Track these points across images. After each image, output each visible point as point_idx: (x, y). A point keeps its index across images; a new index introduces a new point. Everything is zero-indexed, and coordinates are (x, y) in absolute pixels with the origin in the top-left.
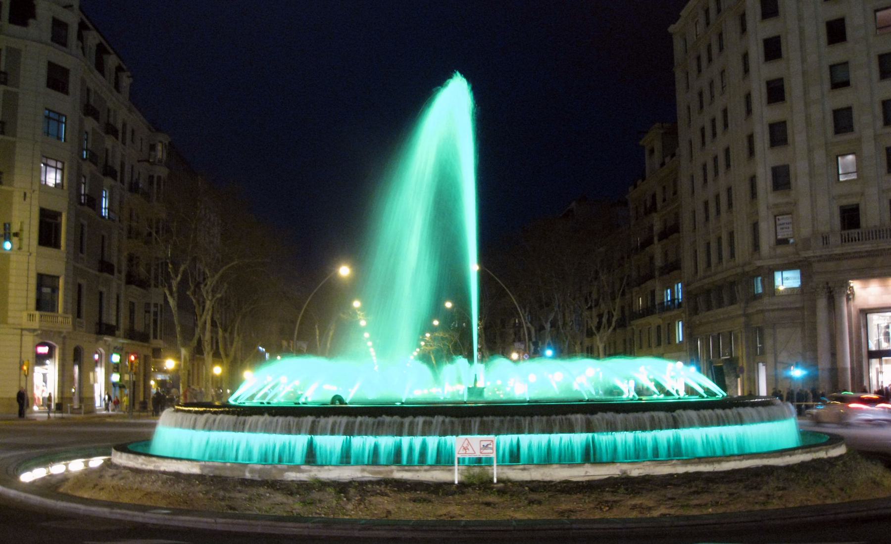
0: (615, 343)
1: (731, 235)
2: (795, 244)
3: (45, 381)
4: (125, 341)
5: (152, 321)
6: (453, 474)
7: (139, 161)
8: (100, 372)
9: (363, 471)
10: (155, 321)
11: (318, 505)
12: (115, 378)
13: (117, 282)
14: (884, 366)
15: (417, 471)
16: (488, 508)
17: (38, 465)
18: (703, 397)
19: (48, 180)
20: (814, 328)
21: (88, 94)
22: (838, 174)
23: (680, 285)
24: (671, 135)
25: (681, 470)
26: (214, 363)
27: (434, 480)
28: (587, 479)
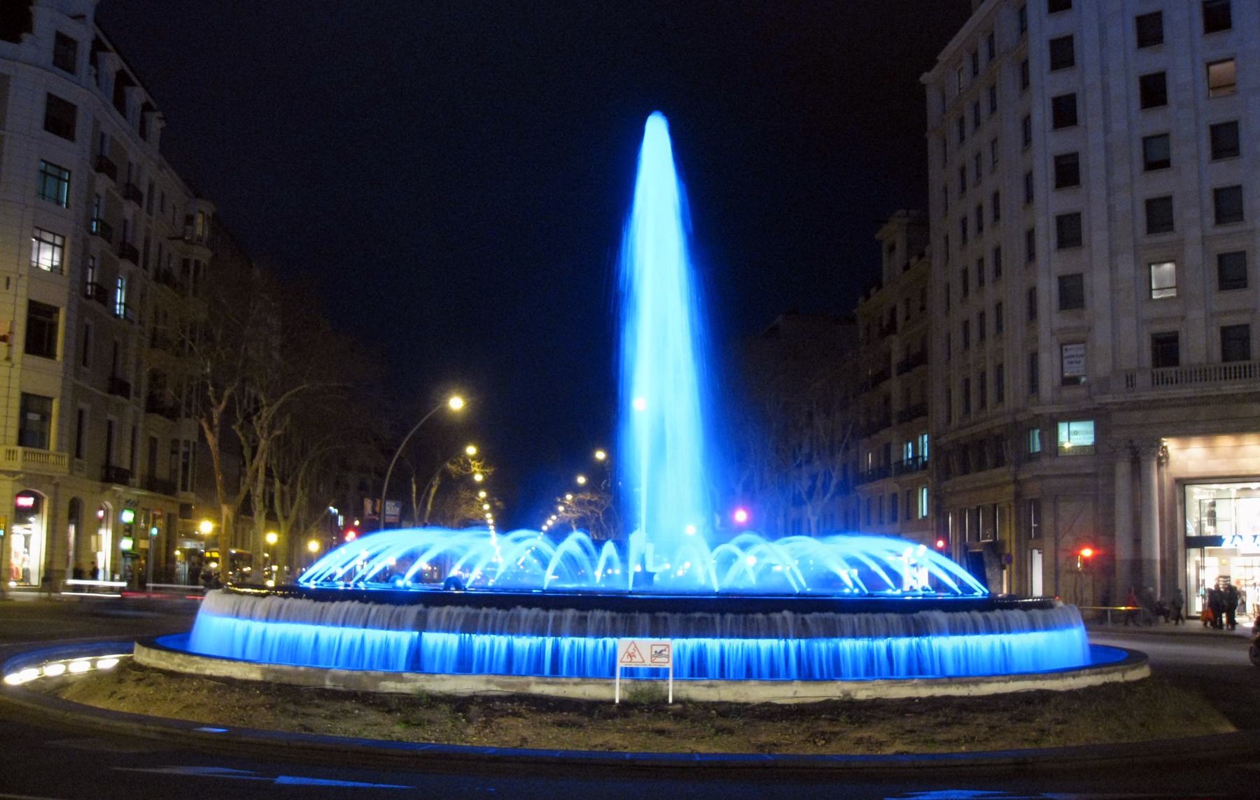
0: (832, 516)
1: (1000, 369)
2: (1088, 385)
3: (27, 546)
4: (145, 493)
5: (180, 464)
6: (614, 689)
7: (170, 238)
8: (106, 535)
9: (489, 682)
10: (185, 467)
11: (427, 727)
12: (127, 544)
13: (132, 409)
14: (1206, 558)
15: (563, 684)
16: (660, 738)
17: (29, 663)
18: (956, 594)
19: (41, 261)
20: (1111, 502)
21: (102, 142)
22: (1151, 290)
23: (926, 437)
24: (920, 228)
25: (924, 692)
26: (267, 528)
27: (586, 697)
28: (795, 701)
